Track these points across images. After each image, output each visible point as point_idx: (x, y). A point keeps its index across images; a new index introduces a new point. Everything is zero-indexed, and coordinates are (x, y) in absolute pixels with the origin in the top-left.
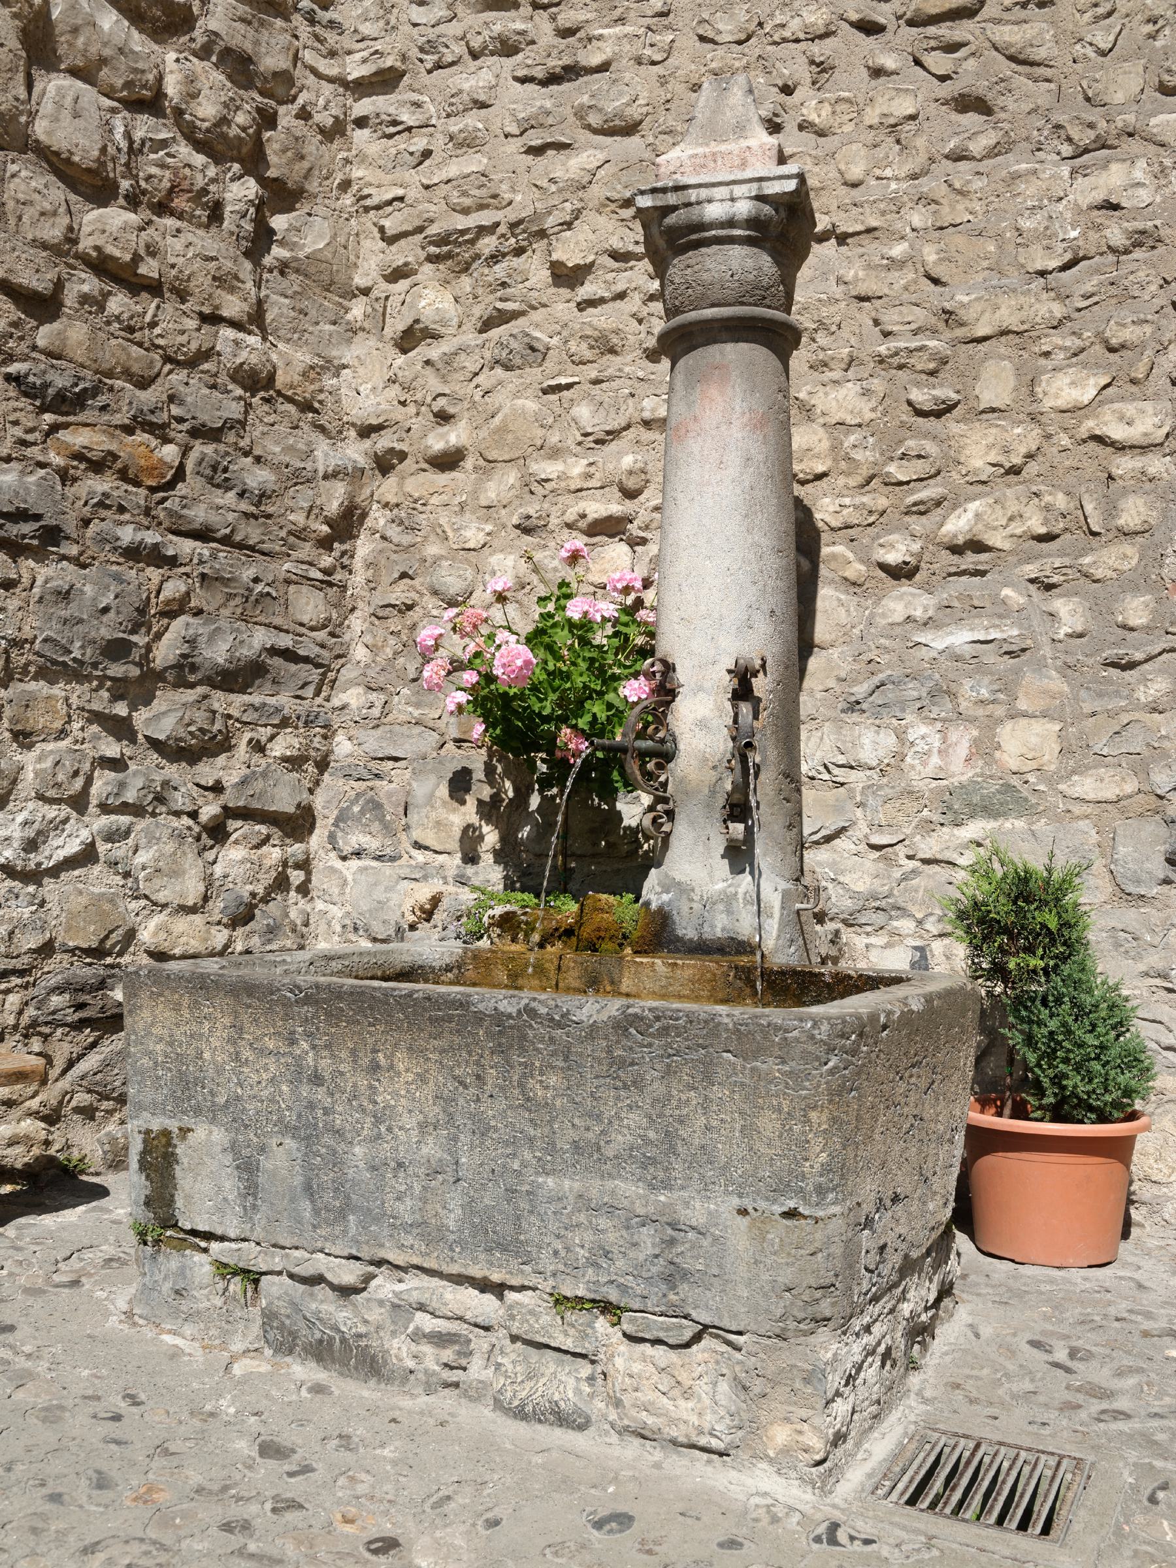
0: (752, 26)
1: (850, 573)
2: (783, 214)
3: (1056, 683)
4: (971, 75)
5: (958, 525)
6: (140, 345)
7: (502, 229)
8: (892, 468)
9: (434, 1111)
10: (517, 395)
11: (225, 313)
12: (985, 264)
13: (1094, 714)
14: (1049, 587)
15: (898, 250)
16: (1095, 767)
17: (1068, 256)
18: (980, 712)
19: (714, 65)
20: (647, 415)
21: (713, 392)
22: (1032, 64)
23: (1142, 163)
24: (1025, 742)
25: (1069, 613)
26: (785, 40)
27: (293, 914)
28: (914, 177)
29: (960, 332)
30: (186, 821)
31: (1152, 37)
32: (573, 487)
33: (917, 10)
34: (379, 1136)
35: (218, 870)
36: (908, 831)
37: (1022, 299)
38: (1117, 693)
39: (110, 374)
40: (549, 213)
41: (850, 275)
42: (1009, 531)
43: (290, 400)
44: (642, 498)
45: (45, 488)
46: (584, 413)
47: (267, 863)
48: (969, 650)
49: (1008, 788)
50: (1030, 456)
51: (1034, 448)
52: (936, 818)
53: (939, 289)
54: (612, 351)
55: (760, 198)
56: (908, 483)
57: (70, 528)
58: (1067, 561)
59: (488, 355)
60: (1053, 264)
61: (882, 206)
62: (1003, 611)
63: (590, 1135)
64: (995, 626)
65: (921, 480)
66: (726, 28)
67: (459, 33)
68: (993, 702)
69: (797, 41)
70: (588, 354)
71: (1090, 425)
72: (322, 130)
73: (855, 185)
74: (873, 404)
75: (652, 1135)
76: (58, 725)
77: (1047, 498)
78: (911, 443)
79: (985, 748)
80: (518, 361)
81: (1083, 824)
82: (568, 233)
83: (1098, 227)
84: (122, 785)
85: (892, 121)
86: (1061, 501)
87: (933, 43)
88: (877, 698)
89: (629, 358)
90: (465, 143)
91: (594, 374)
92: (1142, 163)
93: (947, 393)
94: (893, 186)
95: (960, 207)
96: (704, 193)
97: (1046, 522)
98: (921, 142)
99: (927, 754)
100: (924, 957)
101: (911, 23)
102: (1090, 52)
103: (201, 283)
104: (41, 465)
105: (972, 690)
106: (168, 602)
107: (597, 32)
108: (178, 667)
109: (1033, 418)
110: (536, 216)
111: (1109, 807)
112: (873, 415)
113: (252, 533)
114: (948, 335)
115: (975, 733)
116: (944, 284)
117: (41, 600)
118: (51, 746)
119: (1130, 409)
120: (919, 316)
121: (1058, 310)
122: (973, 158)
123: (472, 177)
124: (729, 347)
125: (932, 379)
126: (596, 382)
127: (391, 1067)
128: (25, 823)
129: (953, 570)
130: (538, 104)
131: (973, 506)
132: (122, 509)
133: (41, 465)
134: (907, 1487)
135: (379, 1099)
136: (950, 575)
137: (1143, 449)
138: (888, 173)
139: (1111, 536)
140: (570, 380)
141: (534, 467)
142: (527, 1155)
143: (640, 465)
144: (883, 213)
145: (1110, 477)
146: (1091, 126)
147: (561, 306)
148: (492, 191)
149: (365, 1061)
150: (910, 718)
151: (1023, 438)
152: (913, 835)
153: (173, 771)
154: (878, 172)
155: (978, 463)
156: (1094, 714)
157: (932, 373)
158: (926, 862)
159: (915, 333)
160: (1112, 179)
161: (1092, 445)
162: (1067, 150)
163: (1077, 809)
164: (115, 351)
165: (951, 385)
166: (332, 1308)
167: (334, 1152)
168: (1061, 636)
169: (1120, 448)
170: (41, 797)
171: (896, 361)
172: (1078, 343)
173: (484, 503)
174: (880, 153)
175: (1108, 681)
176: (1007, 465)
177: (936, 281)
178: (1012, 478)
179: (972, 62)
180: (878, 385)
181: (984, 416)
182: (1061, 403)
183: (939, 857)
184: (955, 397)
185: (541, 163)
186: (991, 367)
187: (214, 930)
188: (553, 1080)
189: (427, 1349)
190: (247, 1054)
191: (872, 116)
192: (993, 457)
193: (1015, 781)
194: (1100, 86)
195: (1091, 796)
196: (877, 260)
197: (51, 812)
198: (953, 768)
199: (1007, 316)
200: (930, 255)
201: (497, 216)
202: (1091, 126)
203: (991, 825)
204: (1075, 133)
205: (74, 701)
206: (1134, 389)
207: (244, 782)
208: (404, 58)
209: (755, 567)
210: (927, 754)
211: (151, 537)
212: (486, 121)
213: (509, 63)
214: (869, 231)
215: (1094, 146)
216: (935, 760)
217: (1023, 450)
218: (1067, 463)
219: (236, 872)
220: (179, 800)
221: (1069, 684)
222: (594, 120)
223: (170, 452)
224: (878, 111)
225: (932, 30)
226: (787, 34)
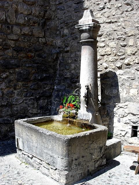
1: (113, 67)
5: (126, 61)
8: (118, 53)
12: (130, 26)
15: (119, 24)
18: (128, 87)
27: (49, 108)
28: (121, 14)
29: (127, 35)
43: (49, 45)
50: (136, 52)
55: (89, 27)
56: (120, 55)
85: (118, 7)
90: (68, 11)
93: (125, 43)
94: (119, 15)
98: (122, 9)
105: (127, 84)
108: (34, 79)
109: (136, 47)
116: (125, 29)
120: (122, 33)
131: (128, 59)
136: (126, 68)
141: (76, 53)
157: (123, 41)
159: (122, 35)
173: (71, 57)
174: (117, 11)
177: (124, 28)
180: (116, 42)
184: (126, 44)
193: (132, 97)
196: (117, 25)
199: (132, 33)
200: (123, 24)
208: (62, 1)
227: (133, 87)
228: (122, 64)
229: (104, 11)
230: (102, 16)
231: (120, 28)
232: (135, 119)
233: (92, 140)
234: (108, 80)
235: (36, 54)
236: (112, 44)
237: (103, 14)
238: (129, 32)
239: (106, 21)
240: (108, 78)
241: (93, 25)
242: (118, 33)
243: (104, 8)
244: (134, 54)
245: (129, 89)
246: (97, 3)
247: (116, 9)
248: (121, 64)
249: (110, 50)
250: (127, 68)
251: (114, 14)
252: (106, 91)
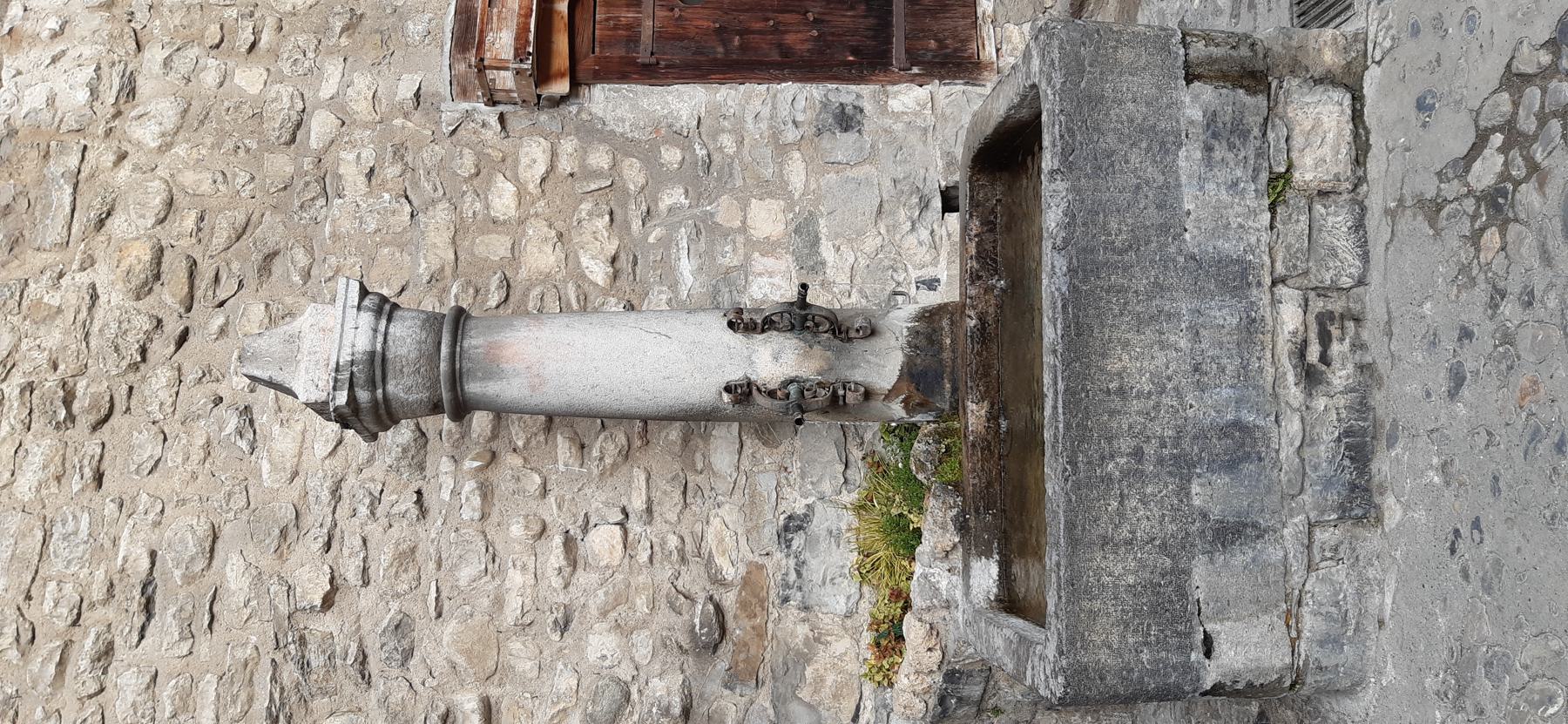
0: (155, 429)
7: (279, 657)
9: (1150, 334)
10: (439, 642)
17: (403, 200)
19: (180, 460)
20: (477, 515)
21: (507, 353)
23: (343, 154)
26: (174, 404)
31: (248, 151)
32: (533, 582)
33: (181, 303)
34: (1176, 389)
40: (276, 608)
44: (548, 519)
46: (466, 574)
54: (413, 550)
59: (396, 672)
60: (408, 209)
62: (667, 242)
63: (1150, 194)
66: (151, 450)
67: (77, 705)
70: (412, 573)
75: (1144, 145)
78: (531, 305)
79: (769, 247)
80: (405, 643)
82: (298, 590)
86: (586, 206)
89: (423, 535)
91: (432, 565)
92: (343, 154)
93: (495, 281)
96: (347, 342)
97: (601, 216)
100: (923, 282)
101: (189, 309)
105: (729, 258)
107: (120, 561)
109: (522, 222)
110: (276, 619)
114: (448, 281)
115: (757, 254)
119: (524, 161)
123: (221, 690)
126: (439, 566)
127: (1119, 374)
130: (170, 619)
135: (1147, 389)
137: (554, 155)
140: (433, 588)
142: (1172, 249)
143: (521, 519)
145: (572, 175)
146: (307, 184)
147: (363, 603)
148: (240, 669)
149: (1117, 403)
151: (537, 230)
155: (553, 258)
160: (350, 169)
161: (547, 186)
162: (321, 201)
165: (489, 278)
166: (1323, 448)
167: (1195, 437)
169: (552, 168)
182: (513, 205)
185: (224, 616)
188: (1114, 225)
189: (1335, 348)
190: (1125, 533)
192: (549, 249)
198: (783, 268)
201: (266, 663)
202: (307, 184)
206: (509, 160)
212: (170, 677)
213: (121, 652)
222: (200, 564)
225: (199, 294)
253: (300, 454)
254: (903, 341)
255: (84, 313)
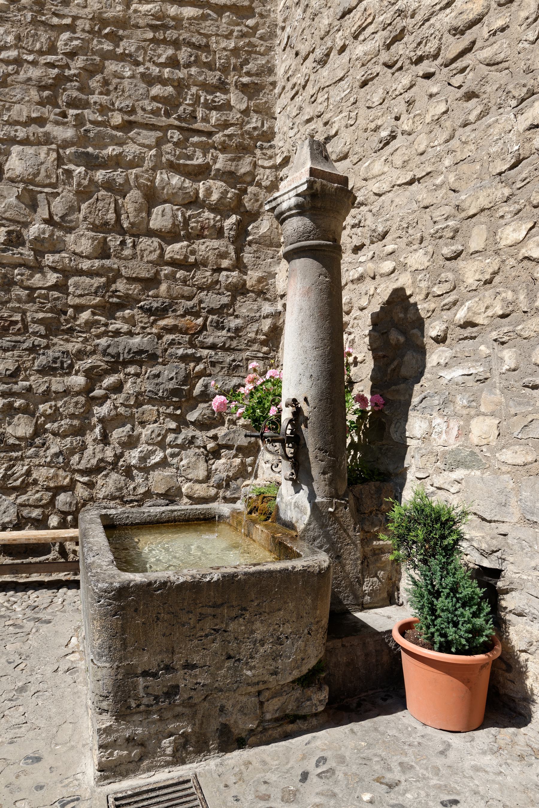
2: (308, 199)
3: (498, 396)
4: (470, 80)
6: (189, 286)
11: (222, 266)
12: (475, 176)
13: (516, 415)
14: (503, 343)
15: (438, 181)
16: (515, 445)
18: (465, 412)
22: (498, 63)
24: (482, 429)
25: (509, 357)
26: (397, 96)
28: (447, 141)
30: (202, 450)
35: (214, 467)
36: (431, 472)
37: (489, 191)
38: (528, 404)
39: (177, 298)
41: (420, 198)
42: (486, 314)
45: (150, 342)
47: (234, 464)
48: (461, 380)
49: (473, 453)
50: (495, 273)
51: (497, 268)
52: (442, 466)
53: (456, 194)
55: (298, 195)
56: (442, 295)
57: (159, 352)
58: (511, 328)
61: (433, 160)
64: (474, 366)
65: (447, 293)
68: (469, 407)
69: (401, 94)
71: (524, 252)
72: (266, 188)
73: (422, 154)
74: (429, 258)
76: (154, 419)
77: (504, 295)
79: (464, 432)
81: (506, 477)
83: (530, 140)
84: (176, 438)
85: (436, 117)
87: (455, 72)
88: (423, 405)
95: (465, 150)
99: (441, 433)
102: (526, 45)
103: (212, 258)
104: (149, 334)
106: (197, 373)
109: (497, 253)
111: (520, 468)
112: (428, 264)
113: (234, 344)
116: (458, 192)
117: (148, 378)
118: (151, 426)
120: (447, 210)
121: (507, 192)
122: (471, 123)
124: (297, 261)
125: (452, 241)
128: (141, 452)
129: (461, 337)
132: (180, 344)
133: (149, 334)
134: (147, 799)
136: (460, 340)
138: (436, 143)
139: (532, 313)
144: (434, 163)
146: (524, 86)
150: (435, 414)
151: (491, 264)
152: (433, 474)
153: (198, 433)
154: (432, 144)
156: (516, 415)
158: (439, 488)
161: (526, 262)
162: (514, 103)
163: (504, 468)
164: (178, 289)
168: (504, 371)
170: (147, 443)
171: (438, 235)
172: (518, 207)
175: (525, 396)
176: (484, 280)
178: (488, 286)
179: (471, 74)
181: (473, 256)
183: (442, 487)
186: (475, 231)
187: (211, 488)
191: (428, 119)
193: (477, 450)
194: (530, 62)
195: (510, 462)
197: (150, 448)
199: (483, 201)
202: (524, 86)
203: (466, 472)
204: (516, 93)
205: (161, 410)
207: (226, 435)
209: (303, 357)
210: (441, 433)
211: (190, 351)
214: (428, 174)
215: (527, 96)
216: (444, 436)
217: (491, 270)
218: (513, 274)
219: (221, 468)
220: (199, 442)
221: (505, 398)
223: (200, 321)
224: (430, 115)
225: (454, 66)
226: (397, 93)
227: (483, 409)
228: (446, 325)
229: (394, 144)
230: (386, 169)
231: (441, 193)
232: (488, 538)
233: (234, 603)
234: (402, 386)
235: (209, 319)
236: (418, 259)
237: (390, 158)
238: (467, 204)
239: (399, 182)
240: (403, 382)
241: (305, 187)
242: (437, 214)
243: (393, 137)
244: (488, 282)
245: (470, 417)
246: (372, 126)
247: (428, 129)
248: (443, 327)
249: (410, 281)
250: (466, 338)
251: (421, 149)
252: (393, 426)
253: (374, 177)
254: (108, 548)
255: (438, 7)
